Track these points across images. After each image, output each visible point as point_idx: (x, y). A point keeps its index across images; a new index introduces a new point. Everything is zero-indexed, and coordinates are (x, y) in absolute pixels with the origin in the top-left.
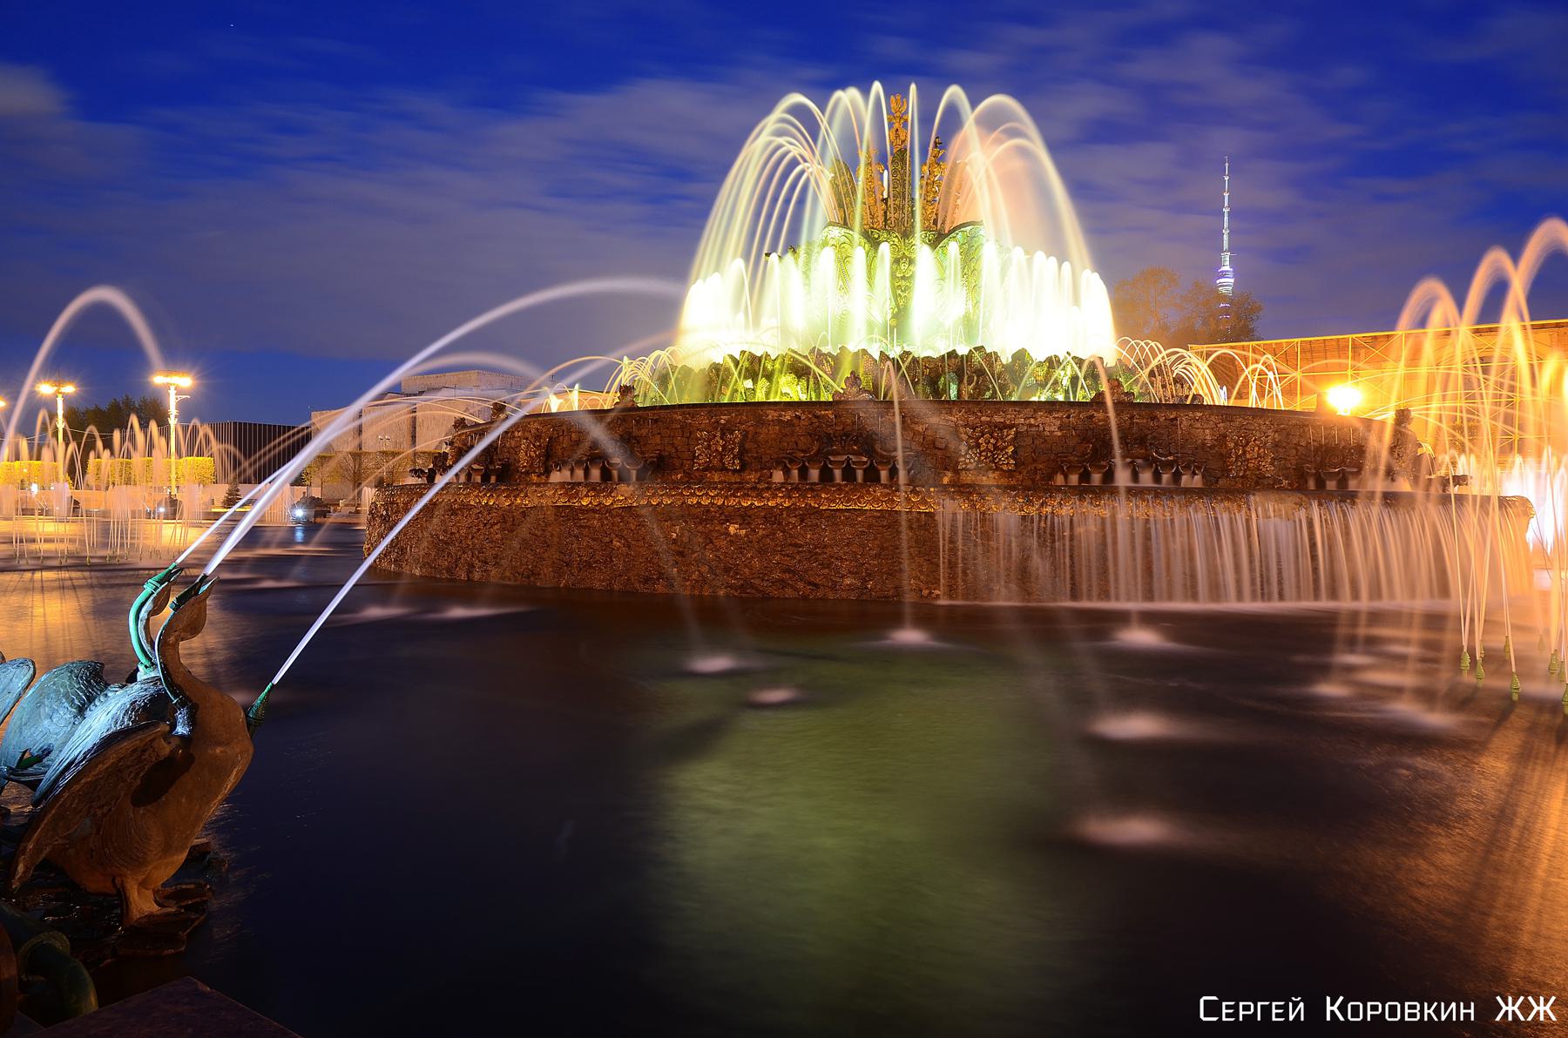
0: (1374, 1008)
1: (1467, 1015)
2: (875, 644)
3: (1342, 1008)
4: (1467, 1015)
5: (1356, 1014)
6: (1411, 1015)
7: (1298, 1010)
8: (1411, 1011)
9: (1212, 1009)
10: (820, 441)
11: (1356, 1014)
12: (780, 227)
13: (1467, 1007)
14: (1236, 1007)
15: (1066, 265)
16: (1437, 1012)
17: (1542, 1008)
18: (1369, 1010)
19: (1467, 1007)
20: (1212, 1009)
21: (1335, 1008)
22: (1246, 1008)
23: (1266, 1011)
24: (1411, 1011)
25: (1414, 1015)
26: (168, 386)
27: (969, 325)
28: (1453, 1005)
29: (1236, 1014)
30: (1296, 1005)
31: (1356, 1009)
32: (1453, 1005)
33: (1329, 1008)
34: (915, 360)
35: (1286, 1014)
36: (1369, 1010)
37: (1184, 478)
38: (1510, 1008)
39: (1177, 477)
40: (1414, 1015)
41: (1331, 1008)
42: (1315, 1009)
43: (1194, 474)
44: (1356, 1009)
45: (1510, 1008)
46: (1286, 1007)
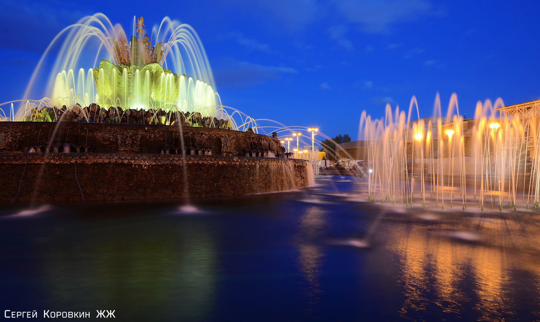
1: (88, 316)
2: (344, 195)
3: (49, 314)
4: (88, 316)
5: (53, 315)
6: (70, 316)
7: (35, 314)
8: (70, 315)
9: (9, 314)
10: (84, 130)
11: (53, 315)
12: (90, 56)
13: (88, 313)
14: (16, 314)
15: (190, 79)
16: (78, 315)
17: (101, 314)
18: (57, 314)
19: (88, 313)
20: (9, 314)
21: (47, 314)
23: (25, 314)
24: (70, 315)
25: (71, 316)
27: (119, 96)
28: (83, 313)
29: (16, 316)
30: (34, 313)
31: (53, 314)
32: (83, 313)
33: (45, 314)
34: (88, 108)
35: (31, 316)
36: (57, 314)
37: (206, 152)
38: (111, 314)
39: (203, 152)
40: (71, 316)
41: (45, 314)
42: (41, 314)
43: (209, 151)
44: (53, 314)
45: (111, 314)
46: (31, 313)
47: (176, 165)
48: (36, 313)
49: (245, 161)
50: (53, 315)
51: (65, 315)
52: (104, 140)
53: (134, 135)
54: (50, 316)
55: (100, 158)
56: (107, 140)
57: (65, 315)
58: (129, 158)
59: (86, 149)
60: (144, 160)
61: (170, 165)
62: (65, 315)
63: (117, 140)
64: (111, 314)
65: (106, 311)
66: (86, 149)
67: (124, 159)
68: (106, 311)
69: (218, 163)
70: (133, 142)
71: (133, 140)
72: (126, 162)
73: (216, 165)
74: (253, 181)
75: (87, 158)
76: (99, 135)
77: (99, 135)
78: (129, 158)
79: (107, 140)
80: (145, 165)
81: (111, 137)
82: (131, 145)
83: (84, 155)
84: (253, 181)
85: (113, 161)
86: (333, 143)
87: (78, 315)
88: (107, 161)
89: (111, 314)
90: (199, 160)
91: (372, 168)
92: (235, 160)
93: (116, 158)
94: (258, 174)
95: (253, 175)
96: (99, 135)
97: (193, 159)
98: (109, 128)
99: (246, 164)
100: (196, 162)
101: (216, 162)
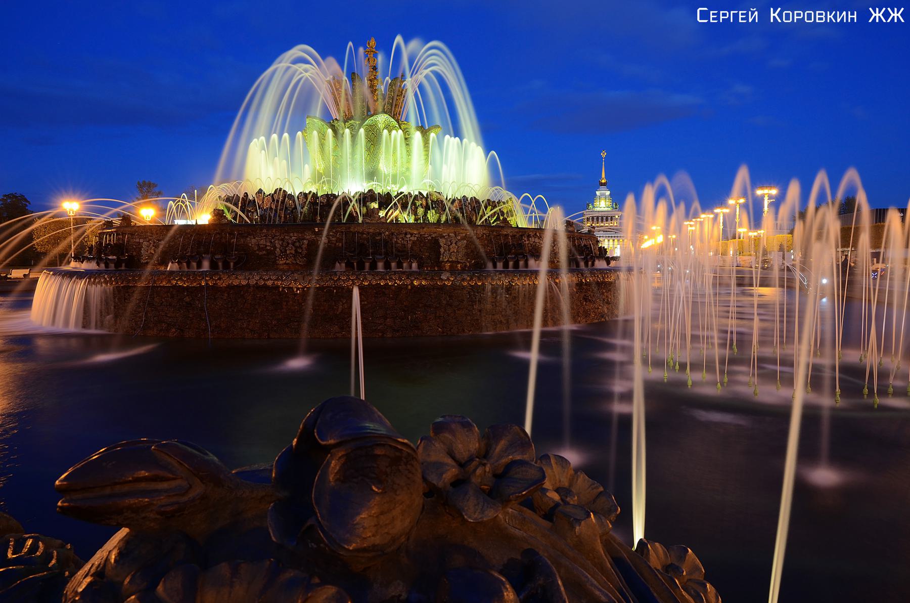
0: (798, 15)
1: (852, 19)
3: (780, 15)
4: (852, 19)
6: (819, 19)
9: (705, 15)
13: (852, 14)
14: (718, 14)
16: (835, 17)
18: (796, 16)
19: (852, 14)
21: (776, 15)
22: (724, 15)
23: (736, 16)
25: (822, 19)
26: (763, 196)
28: (844, 13)
29: (718, 18)
30: (753, 13)
31: (787, 16)
32: (844, 13)
33: (772, 15)
35: (747, 18)
36: (796, 16)
40: (822, 19)
41: (773, 15)
42: (764, 15)
45: (896, 15)
46: (747, 14)
47: (343, 288)
48: (756, 13)
49: (463, 280)
50: (787, 16)
51: (809, 18)
52: (260, 249)
53: (299, 240)
54: (781, 19)
55: (237, 278)
56: (263, 249)
57: (809, 18)
58: (274, 277)
59: (232, 264)
60: (295, 280)
61: (335, 288)
62: (809, 16)
63: (275, 248)
64: (896, 15)
65: (886, 10)
66: (232, 264)
67: (268, 280)
68: (886, 10)
69: (412, 283)
70: (296, 251)
71: (296, 247)
72: (269, 283)
73: (409, 287)
74: (480, 311)
75: (220, 279)
76: (253, 241)
77: (253, 242)
78: (274, 277)
79: (263, 249)
80: (298, 289)
81: (268, 244)
82: (294, 256)
83: (217, 274)
84: (480, 311)
85: (252, 282)
86: (317, 251)
87: (835, 17)
88: (244, 283)
89: (896, 15)
90: (380, 279)
91: (823, 286)
92: (444, 277)
93: (257, 278)
94: (489, 300)
95: (479, 301)
96: (253, 242)
97: (369, 277)
98: (265, 231)
99: (465, 284)
100: (374, 283)
101: (409, 282)
